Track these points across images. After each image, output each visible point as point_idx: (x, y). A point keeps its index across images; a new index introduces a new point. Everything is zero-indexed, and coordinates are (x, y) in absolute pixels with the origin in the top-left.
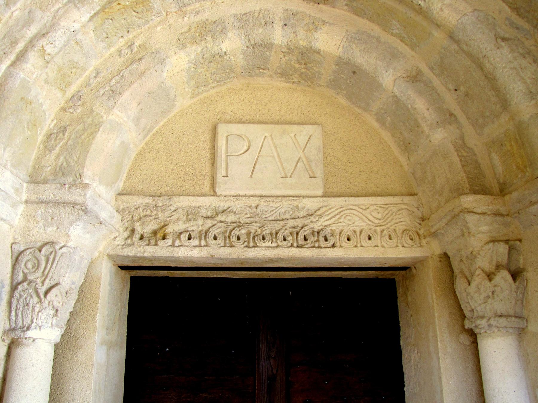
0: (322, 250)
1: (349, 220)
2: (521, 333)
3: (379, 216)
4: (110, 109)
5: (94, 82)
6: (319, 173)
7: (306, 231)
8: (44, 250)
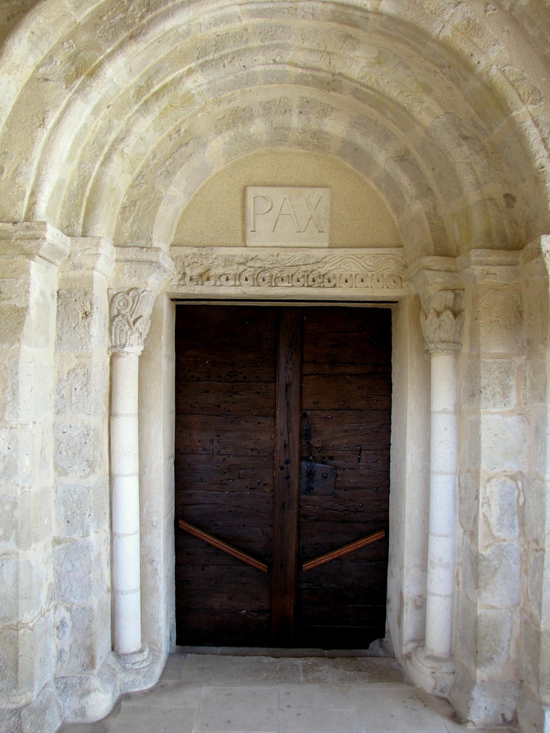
0: (326, 289)
1: (348, 266)
2: (457, 353)
3: (371, 264)
4: (167, 187)
5: (152, 163)
6: (326, 229)
7: (315, 274)
8: (131, 293)
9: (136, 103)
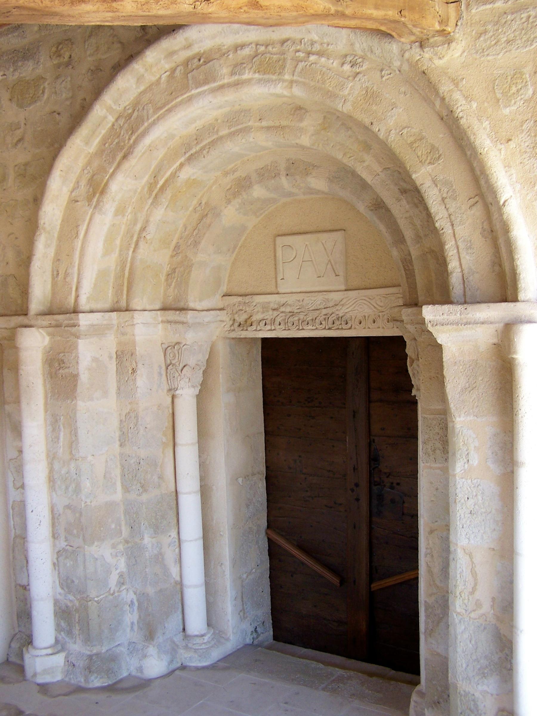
3: (382, 304)
8: (176, 347)
9: (149, 198)
